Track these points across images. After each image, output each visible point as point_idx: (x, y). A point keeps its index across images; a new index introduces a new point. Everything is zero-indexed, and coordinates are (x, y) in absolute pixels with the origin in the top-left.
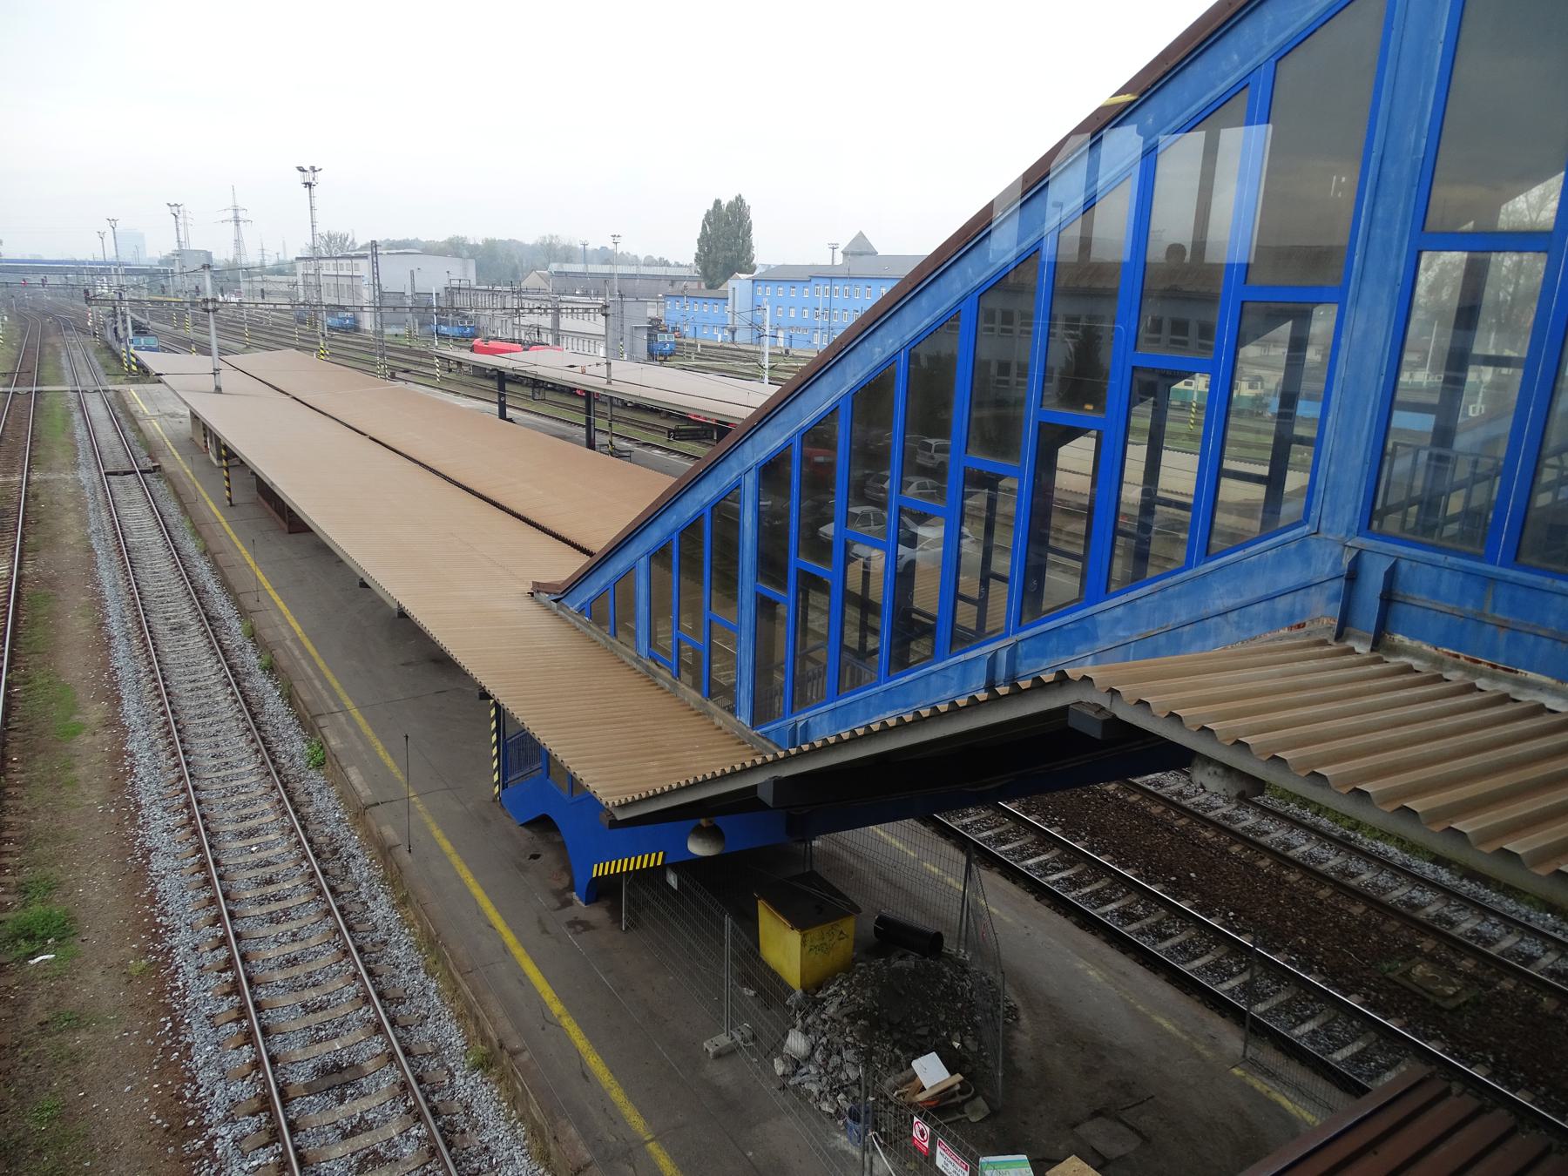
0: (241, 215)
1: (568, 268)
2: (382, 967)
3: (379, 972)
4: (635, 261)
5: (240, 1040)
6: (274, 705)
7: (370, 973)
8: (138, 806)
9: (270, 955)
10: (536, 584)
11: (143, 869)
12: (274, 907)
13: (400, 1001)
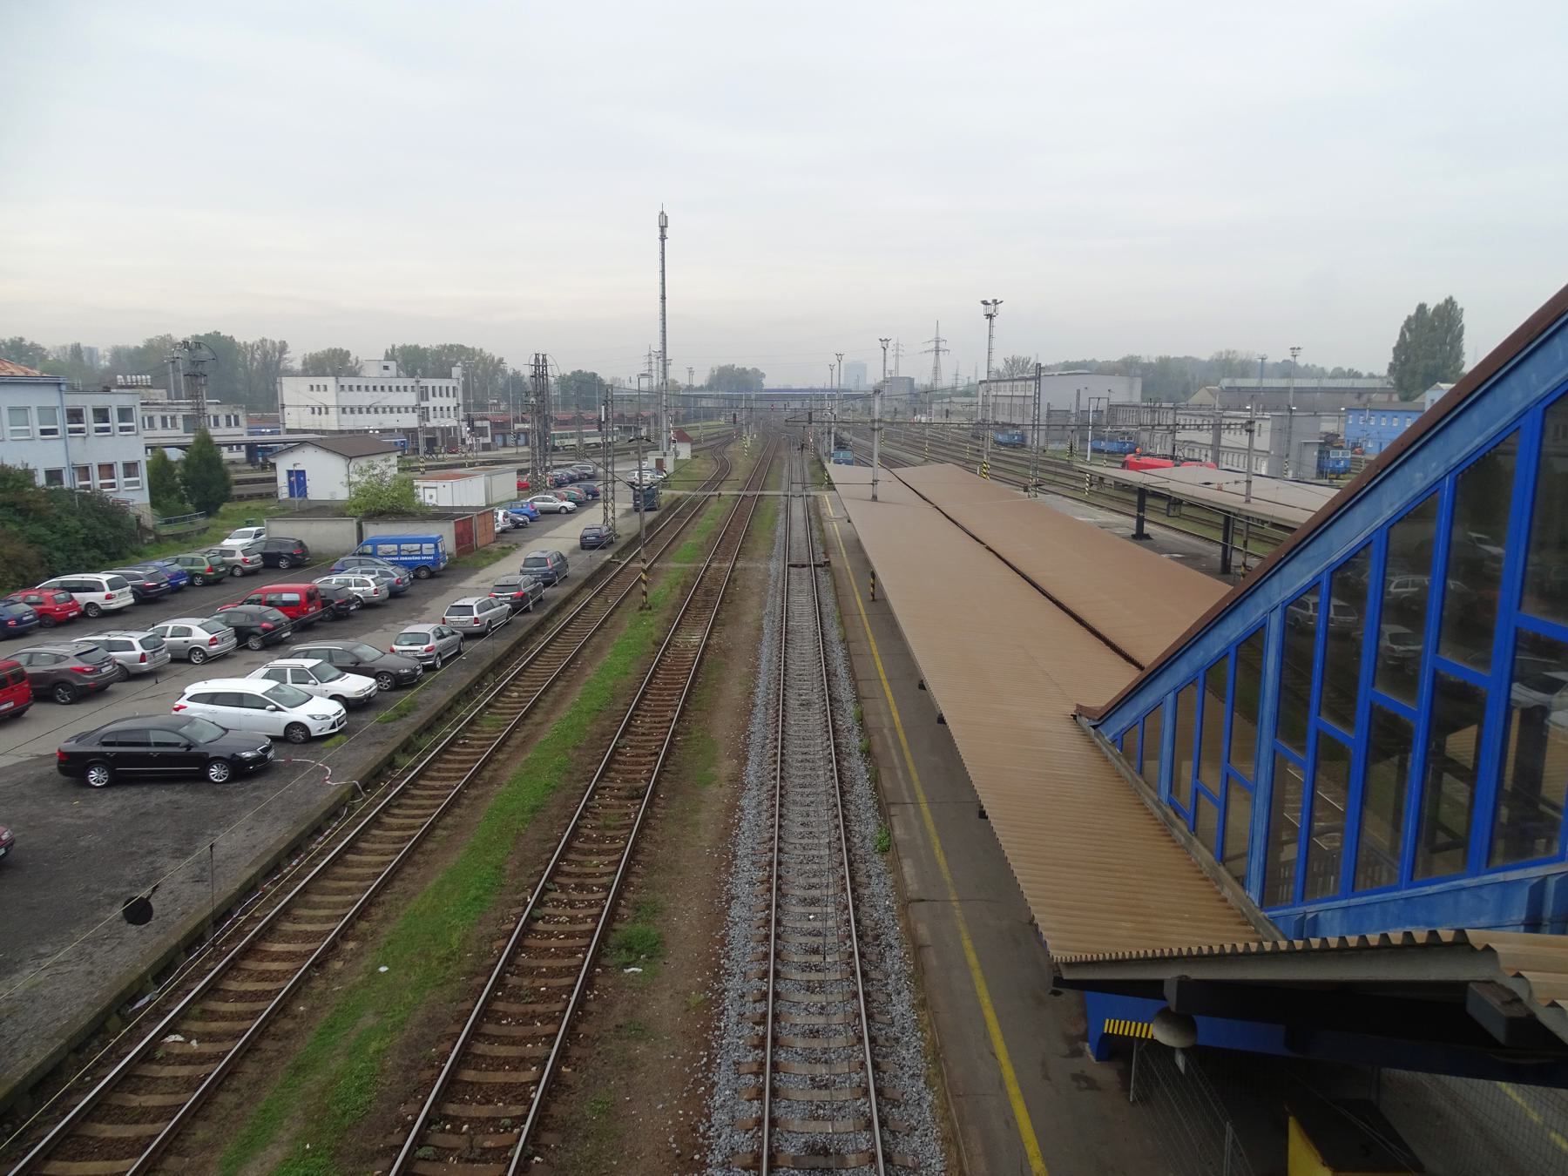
0: (942, 345)
1: (1240, 382)
2: (888, 1065)
3: (884, 1068)
4: (1321, 374)
5: (753, 1095)
6: (862, 788)
7: (876, 1066)
8: (735, 856)
9: (798, 1021)
10: (1079, 707)
11: (724, 912)
12: (814, 976)
13: (895, 1103)
